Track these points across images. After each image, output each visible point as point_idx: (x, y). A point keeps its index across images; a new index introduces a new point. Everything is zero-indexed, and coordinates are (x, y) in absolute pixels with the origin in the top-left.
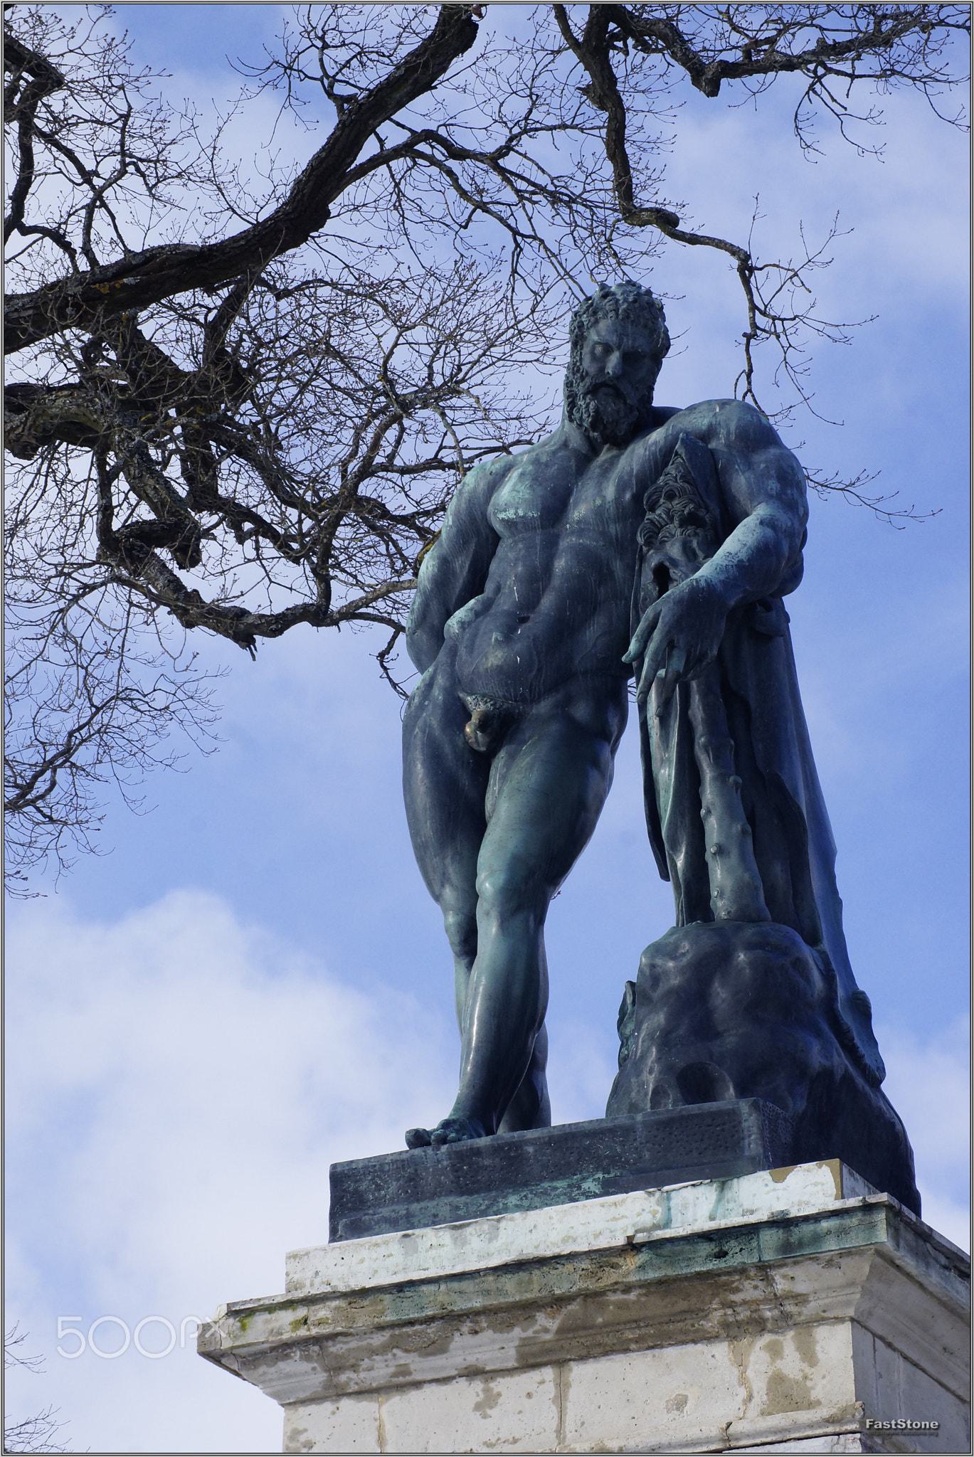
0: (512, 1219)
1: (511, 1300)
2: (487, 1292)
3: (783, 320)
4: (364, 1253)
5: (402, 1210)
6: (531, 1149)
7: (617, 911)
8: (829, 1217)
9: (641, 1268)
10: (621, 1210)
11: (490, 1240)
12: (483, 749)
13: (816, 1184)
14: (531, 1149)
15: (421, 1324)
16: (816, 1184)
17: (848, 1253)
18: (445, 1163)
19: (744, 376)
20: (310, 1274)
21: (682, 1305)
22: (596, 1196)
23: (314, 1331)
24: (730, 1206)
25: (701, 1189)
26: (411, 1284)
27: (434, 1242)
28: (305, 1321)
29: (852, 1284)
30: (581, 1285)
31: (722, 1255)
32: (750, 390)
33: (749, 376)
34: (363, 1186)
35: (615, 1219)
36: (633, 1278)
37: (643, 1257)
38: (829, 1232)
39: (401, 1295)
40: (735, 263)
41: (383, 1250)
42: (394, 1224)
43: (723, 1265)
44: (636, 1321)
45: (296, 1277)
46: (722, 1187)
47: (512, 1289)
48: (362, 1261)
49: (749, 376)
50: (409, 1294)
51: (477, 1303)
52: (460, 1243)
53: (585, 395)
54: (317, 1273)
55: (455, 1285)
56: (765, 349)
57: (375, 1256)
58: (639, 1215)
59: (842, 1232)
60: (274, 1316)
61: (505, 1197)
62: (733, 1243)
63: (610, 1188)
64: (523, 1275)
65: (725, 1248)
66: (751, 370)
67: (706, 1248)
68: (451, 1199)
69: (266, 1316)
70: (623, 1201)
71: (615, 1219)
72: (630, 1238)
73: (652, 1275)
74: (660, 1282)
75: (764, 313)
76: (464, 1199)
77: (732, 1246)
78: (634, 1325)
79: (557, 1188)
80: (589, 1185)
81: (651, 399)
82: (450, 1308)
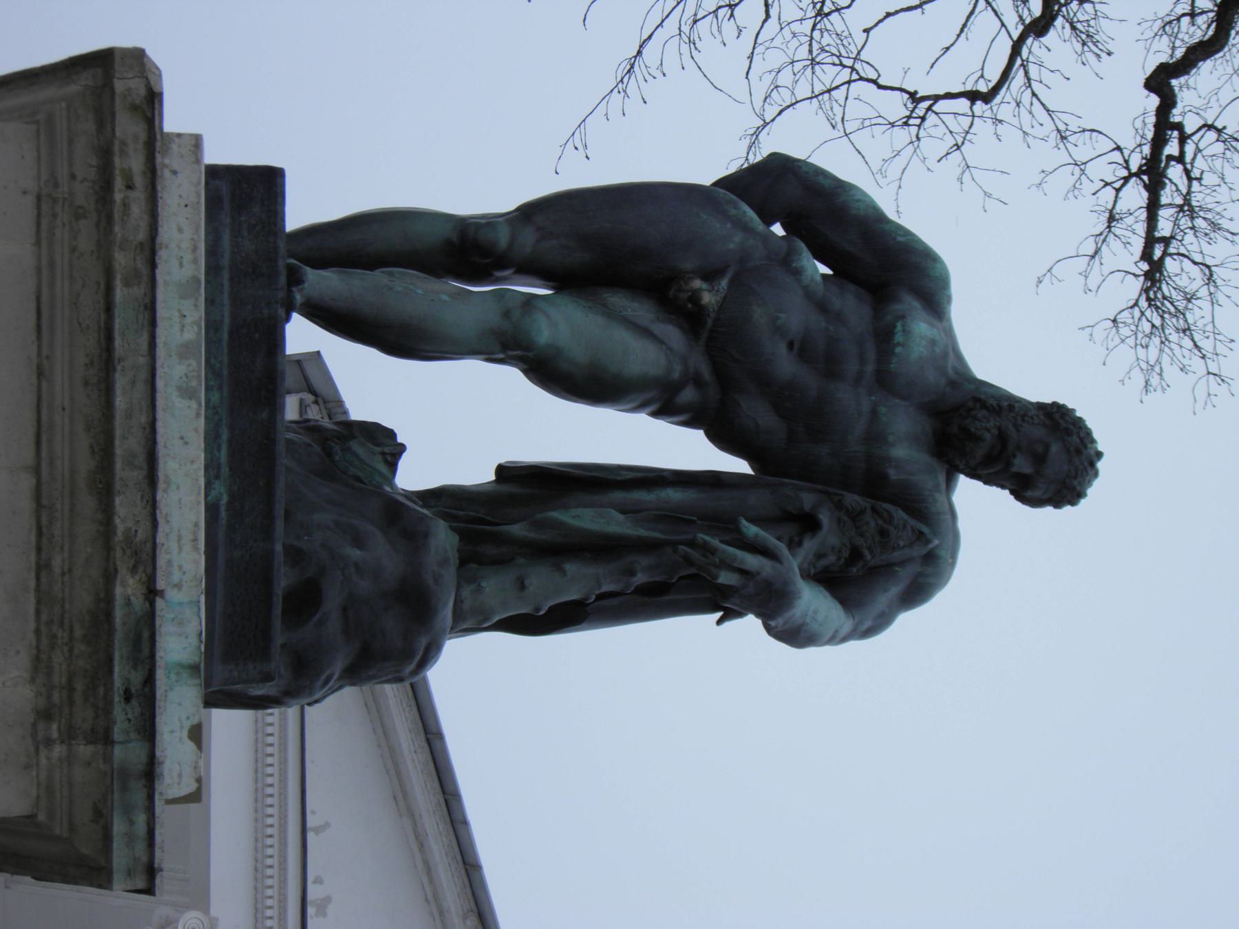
0: (198, 415)
1: (117, 443)
2: (129, 416)
3: (919, 126)
4: (188, 233)
5: (226, 262)
6: (264, 415)
7: (457, 421)
8: (148, 824)
9: (128, 602)
10: (187, 547)
11: (179, 388)
12: (671, 294)
13: (180, 776)
14: (264, 415)
15: (106, 323)
16: (180, 776)
17: (107, 837)
18: (266, 311)
19: (873, 76)
20: (175, 166)
21: (78, 633)
22: (206, 495)
23: (118, 197)
24: (173, 676)
25: (194, 640)
26: (153, 323)
27: (189, 320)
28: (130, 187)
29: (72, 828)
30: (120, 528)
31: (128, 696)
32: (861, 79)
33: (874, 82)
34: (256, 209)
35: (180, 538)
36: (118, 591)
37: (138, 603)
38: (132, 823)
39: (142, 308)
40: (983, 88)
41: (188, 257)
42: (213, 251)
43: (116, 699)
44: (70, 570)
45: (175, 147)
46: (194, 668)
47: (127, 443)
48: (180, 230)
49: (874, 82)
50: (141, 317)
51: (120, 402)
52: (185, 351)
53: (999, 429)
54: (175, 173)
55: (143, 375)
56: (896, 106)
57: (184, 245)
58: (180, 567)
59: (130, 839)
60: (140, 146)
61: (220, 388)
62: (138, 710)
63: (212, 510)
64: (141, 460)
65: (134, 702)
66: (880, 87)
67: (137, 678)
68: (227, 320)
69: (143, 136)
70: (196, 549)
71: (180, 538)
72: (161, 593)
73: (119, 613)
74: (109, 615)
75: (929, 109)
76: (226, 336)
77: (135, 709)
78: (66, 569)
79: (219, 450)
80: (220, 488)
81: (973, 475)
82: (119, 368)
